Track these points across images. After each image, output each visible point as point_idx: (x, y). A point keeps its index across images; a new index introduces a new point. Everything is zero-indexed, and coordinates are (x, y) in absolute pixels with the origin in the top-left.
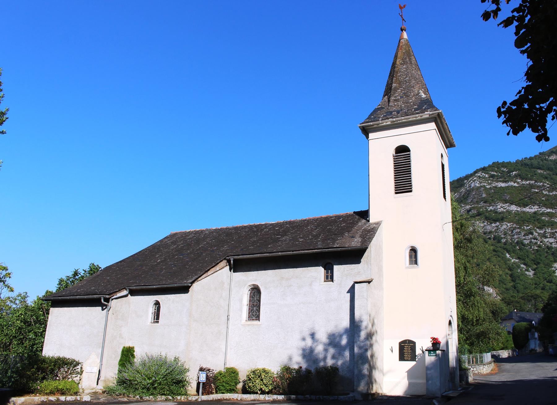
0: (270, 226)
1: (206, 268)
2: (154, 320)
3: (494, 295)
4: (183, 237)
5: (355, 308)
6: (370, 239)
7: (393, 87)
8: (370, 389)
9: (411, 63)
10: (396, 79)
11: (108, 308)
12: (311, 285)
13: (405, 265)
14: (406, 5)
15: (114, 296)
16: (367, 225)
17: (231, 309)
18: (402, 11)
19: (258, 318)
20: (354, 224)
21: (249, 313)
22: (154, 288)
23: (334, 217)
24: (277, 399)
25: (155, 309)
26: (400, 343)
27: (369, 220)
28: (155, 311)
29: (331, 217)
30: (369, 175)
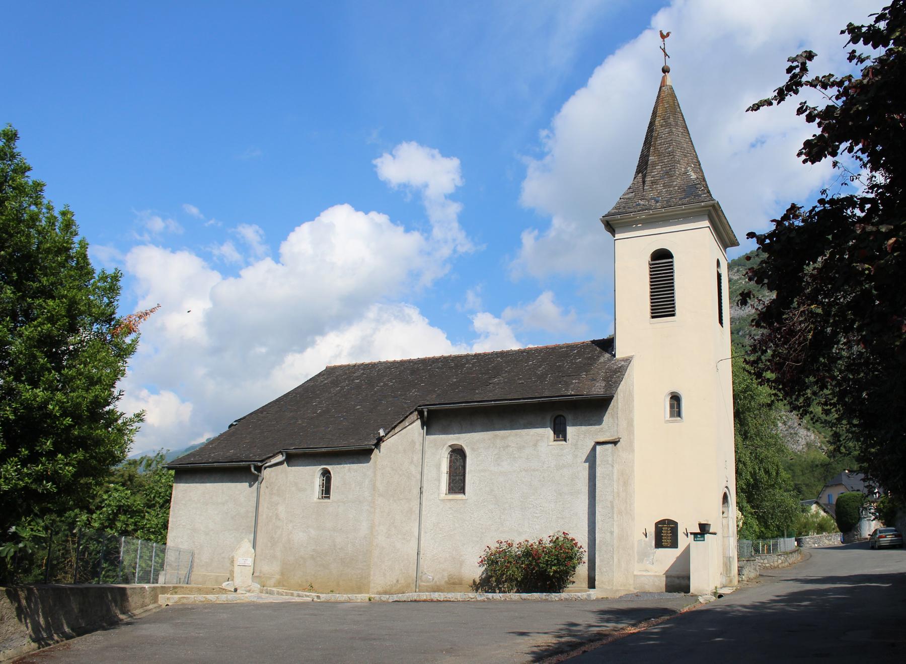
0: (474, 359)
1: (393, 424)
2: (322, 494)
3: (817, 443)
4: (346, 373)
5: (597, 478)
6: (617, 383)
7: (650, 161)
8: (581, 635)
9: (677, 125)
10: (655, 149)
11: (260, 479)
12: (535, 445)
13: (665, 417)
14: (670, 32)
15: (266, 463)
16: (613, 362)
17: (425, 478)
18: (664, 41)
19: (462, 491)
20: (593, 360)
21: (449, 485)
22: (323, 452)
23: (564, 348)
24: (493, 598)
25: (323, 480)
26: (657, 524)
27: (615, 354)
28: (323, 483)
29: (561, 348)
30: (615, 291)
